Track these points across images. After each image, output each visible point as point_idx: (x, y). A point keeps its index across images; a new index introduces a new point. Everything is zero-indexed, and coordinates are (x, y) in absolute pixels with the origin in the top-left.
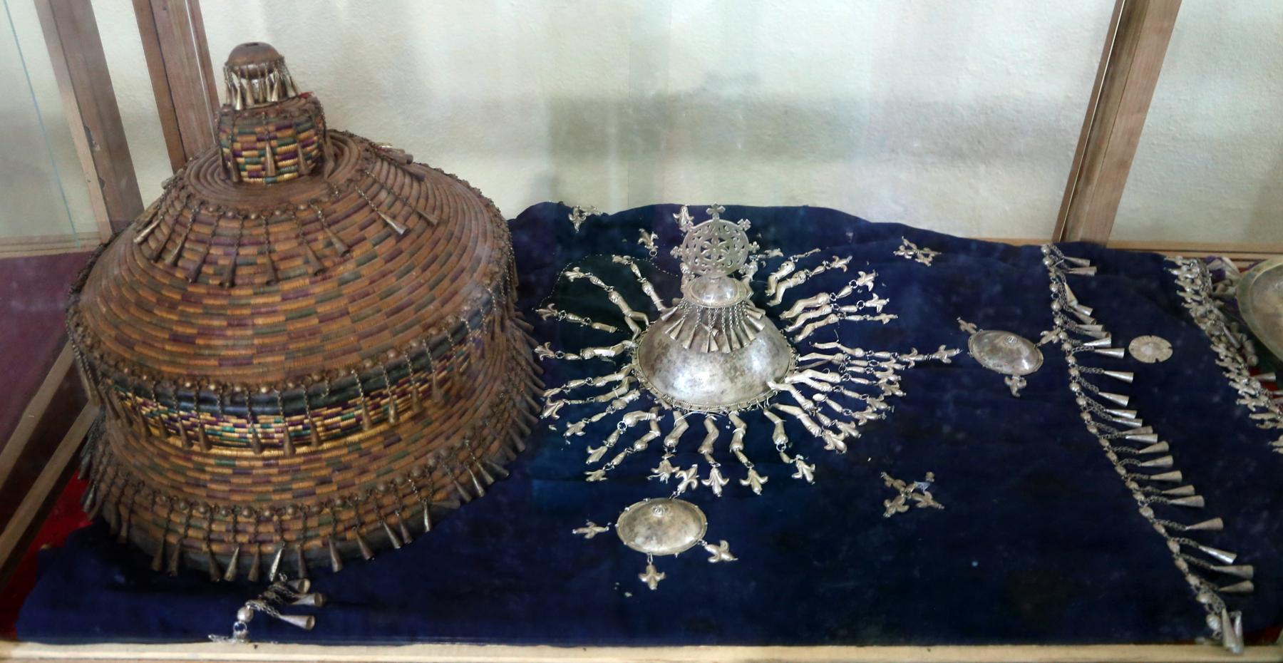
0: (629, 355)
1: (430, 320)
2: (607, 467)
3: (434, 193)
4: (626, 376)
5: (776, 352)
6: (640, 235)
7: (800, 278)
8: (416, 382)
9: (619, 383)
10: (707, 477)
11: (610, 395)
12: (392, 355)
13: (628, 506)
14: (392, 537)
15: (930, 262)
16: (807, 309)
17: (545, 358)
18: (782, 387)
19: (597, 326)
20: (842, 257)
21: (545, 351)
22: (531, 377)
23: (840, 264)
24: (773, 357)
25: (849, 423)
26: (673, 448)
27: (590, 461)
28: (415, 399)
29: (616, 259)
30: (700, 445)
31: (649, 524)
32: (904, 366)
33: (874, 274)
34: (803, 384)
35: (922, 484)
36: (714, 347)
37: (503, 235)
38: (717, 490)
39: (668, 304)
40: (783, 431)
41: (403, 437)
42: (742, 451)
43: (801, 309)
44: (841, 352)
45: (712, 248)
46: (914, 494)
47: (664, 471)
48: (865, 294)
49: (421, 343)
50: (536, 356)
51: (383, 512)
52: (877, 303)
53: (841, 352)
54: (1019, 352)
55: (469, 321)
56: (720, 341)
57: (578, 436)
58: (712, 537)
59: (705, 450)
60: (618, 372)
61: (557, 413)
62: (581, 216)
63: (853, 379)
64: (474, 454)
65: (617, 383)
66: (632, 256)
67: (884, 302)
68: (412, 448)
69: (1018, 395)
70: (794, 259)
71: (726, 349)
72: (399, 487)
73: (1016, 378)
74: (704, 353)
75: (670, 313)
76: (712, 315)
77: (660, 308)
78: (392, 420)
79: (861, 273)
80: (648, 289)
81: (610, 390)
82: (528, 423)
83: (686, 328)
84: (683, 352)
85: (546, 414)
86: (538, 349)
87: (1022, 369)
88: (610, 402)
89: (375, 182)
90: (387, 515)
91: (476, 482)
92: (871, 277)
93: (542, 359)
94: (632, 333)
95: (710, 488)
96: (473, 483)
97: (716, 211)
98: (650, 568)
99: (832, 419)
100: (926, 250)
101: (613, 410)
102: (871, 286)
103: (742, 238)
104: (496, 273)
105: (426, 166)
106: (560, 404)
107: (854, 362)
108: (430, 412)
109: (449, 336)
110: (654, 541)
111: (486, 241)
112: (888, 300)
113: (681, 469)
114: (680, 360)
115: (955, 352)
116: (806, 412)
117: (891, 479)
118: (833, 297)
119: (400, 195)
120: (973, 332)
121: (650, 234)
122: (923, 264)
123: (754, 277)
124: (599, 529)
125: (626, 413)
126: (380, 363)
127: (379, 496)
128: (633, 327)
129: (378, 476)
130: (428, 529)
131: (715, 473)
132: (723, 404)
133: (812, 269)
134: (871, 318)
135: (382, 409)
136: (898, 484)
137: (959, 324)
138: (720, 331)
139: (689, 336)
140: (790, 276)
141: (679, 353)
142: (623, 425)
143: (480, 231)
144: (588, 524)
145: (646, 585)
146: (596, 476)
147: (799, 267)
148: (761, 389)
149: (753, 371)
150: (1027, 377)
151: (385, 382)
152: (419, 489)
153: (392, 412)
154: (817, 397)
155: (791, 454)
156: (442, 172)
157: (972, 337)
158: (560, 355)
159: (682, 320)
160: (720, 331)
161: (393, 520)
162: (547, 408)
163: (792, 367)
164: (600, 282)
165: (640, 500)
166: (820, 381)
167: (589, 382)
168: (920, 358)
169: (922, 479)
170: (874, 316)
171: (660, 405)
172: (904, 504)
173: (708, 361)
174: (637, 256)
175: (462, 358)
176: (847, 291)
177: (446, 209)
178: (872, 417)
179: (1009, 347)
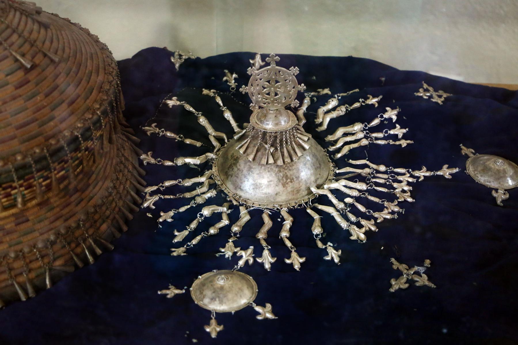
0: (211, 163)
1: (50, 133)
2: (188, 246)
3: (58, 38)
4: (207, 179)
5: (318, 167)
6: (225, 75)
7: (342, 111)
8: (39, 179)
9: (201, 184)
10: (260, 256)
11: (194, 193)
12: (19, 158)
14: (20, 292)
15: (442, 102)
16: (345, 135)
18: (321, 192)
19: (188, 141)
20: (374, 97)
21: (147, 158)
22: (135, 177)
23: (373, 101)
24: (316, 169)
25: (370, 220)
26: (237, 234)
27: (176, 240)
28: (38, 191)
29: (205, 92)
30: (258, 231)
31: (214, 289)
32: (415, 180)
33: (398, 110)
34: (337, 190)
35: (421, 268)
36: (271, 161)
37: (112, 72)
38: (267, 266)
39: (241, 127)
40: (320, 225)
41: (31, 218)
45: (270, 88)
46: (413, 276)
47: (228, 251)
48: (390, 124)
49: (42, 150)
50: (141, 162)
51: (13, 273)
52: (399, 131)
54: (504, 172)
55: (81, 135)
56: (276, 157)
57: (168, 222)
58: (260, 301)
59: (261, 235)
61: (154, 205)
62: (180, 59)
63: (376, 188)
64: (87, 233)
65: (200, 184)
67: (404, 131)
68: (38, 226)
69: (502, 204)
70: (338, 96)
71: (280, 162)
72: (27, 255)
73: (501, 191)
75: (241, 134)
76: (270, 137)
77: (236, 129)
78: (20, 206)
79: (388, 109)
80: (228, 115)
81: (195, 189)
82: (131, 211)
84: (249, 163)
85: (145, 205)
86: (143, 157)
87: (507, 185)
88: (193, 198)
89: (8, 27)
90: (16, 276)
91: (87, 253)
92: (395, 112)
94: (214, 147)
95: (262, 265)
96: (86, 254)
97: (273, 60)
98: (213, 322)
99: (357, 217)
100: (441, 92)
101: (195, 204)
102: (394, 118)
103: (292, 81)
104: (104, 100)
105: (56, 15)
106: (156, 198)
107: (378, 175)
108: (52, 200)
109: (65, 145)
110: (217, 302)
111: (98, 76)
112: (407, 129)
113: (241, 250)
114: (246, 169)
115: (455, 170)
116: (338, 211)
117: (398, 264)
118: (366, 126)
119: (29, 37)
120: (471, 155)
122: (437, 103)
123: (307, 109)
124: (177, 291)
125: (204, 206)
126: (10, 163)
127: (9, 261)
128: (215, 143)
129: (10, 246)
130: (48, 286)
131: (266, 253)
132: (277, 202)
133: (351, 105)
134: (393, 143)
135: (13, 197)
136: (403, 267)
137: (461, 149)
138: (276, 149)
139: (253, 151)
140: (334, 109)
141: (245, 163)
142: (202, 215)
143: (94, 68)
144: (170, 287)
145: (209, 334)
146: (179, 252)
147: (341, 103)
148: (306, 192)
149: (300, 179)
150: (508, 191)
151: (13, 178)
152: (42, 257)
153: (19, 200)
154: (348, 200)
155: (324, 241)
156: (69, 21)
157: (470, 160)
159: (248, 140)
160: (276, 149)
161: (21, 279)
162: (146, 200)
163: (330, 177)
166: (351, 188)
167: (180, 182)
168: (428, 174)
169: (421, 264)
170: (395, 141)
171: (231, 201)
172: (406, 283)
173: (267, 171)
174: (221, 90)
175: (77, 162)
176: (376, 122)
177: (67, 50)
178: (388, 217)
179: (497, 168)
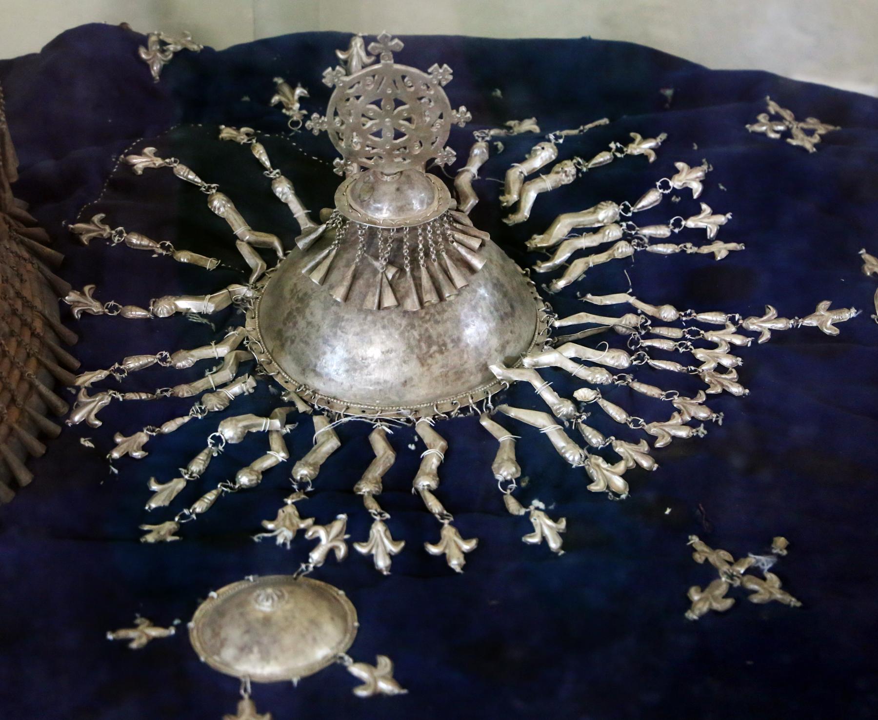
0: (241, 310)
2: (184, 517)
13: (215, 590)
15: (815, 145)
16: (577, 232)
17: (84, 313)
18: (516, 375)
19: (184, 257)
20: (645, 137)
23: (643, 147)
24: (502, 319)
25: (637, 442)
26: (307, 483)
29: (227, 132)
35: (762, 558)
36: (389, 300)
38: (382, 563)
39: (315, 218)
40: (513, 457)
42: (376, 497)
43: (566, 231)
44: (633, 310)
46: (745, 579)
50: (66, 312)
53: (633, 310)
59: (367, 487)
60: (219, 341)
61: (97, 416)
63: (652, 362)
65: (216, 363)
66: (255, 129)
67: (722, 219)
70: (557, 138)
71: (411, 303)
74: (370, 311)
79: (680, 165)
80: (283, 190)
81: (202, 376)
82: (43, 436)
83: (341, 263)
84: (334, 308)
88: (198, 398)
92: (699, 173)
93: (77, 316)
94: (249, 271)
95: (369, 559)
99: (606, 436)
100: (812, 122)
102: (697, 188)
106: (103, 400)
107: (658, 330)
110: (255, 656)
112: (729, 216)
113: (316, 523)
116: (558, 421)
118: (626, 209)
121: (293, 87)
122: (802, 149)
123: (480, 170)
124: (156, 632)
128: (252, 260)
131: (378, 530)
132: (407, 404)
133: (588, 158)
134: (695, 250)
136: (719, 558)
137: (863, 262)
138: (401, 270)
140: (547, 169)
141: (326, 308)
142: (218, 440)
144: (138, 621)
147: (564, 153)
148: (479, 377)
149: (462, 345)
154: (583, 394)
155: (523, 498)
158: (111, 309)
160: (401, 270)
162: (79, 406)
163: (539, 339)
164: (192, 176)
165: (240, 577)
167: (164, 359)
168: (781, 325)
169: (764, 549)
171: (292, 404)
172: (726, 597)
173: (379, 325)
176: (651, 199)
178: (683, 433)
